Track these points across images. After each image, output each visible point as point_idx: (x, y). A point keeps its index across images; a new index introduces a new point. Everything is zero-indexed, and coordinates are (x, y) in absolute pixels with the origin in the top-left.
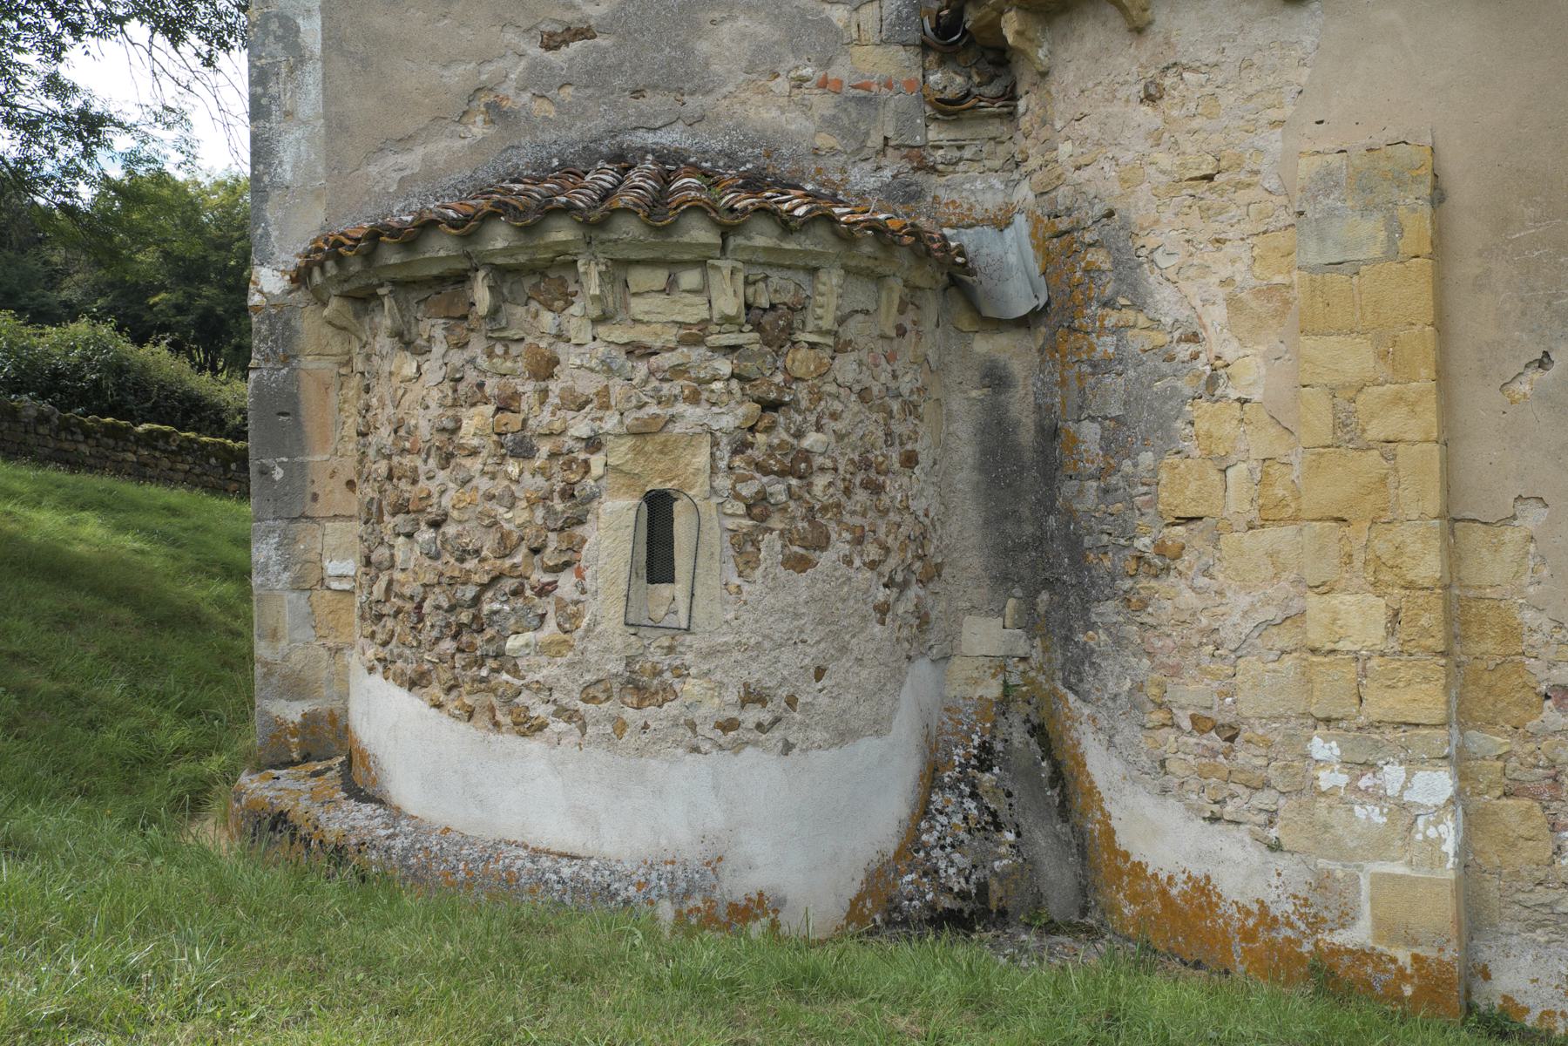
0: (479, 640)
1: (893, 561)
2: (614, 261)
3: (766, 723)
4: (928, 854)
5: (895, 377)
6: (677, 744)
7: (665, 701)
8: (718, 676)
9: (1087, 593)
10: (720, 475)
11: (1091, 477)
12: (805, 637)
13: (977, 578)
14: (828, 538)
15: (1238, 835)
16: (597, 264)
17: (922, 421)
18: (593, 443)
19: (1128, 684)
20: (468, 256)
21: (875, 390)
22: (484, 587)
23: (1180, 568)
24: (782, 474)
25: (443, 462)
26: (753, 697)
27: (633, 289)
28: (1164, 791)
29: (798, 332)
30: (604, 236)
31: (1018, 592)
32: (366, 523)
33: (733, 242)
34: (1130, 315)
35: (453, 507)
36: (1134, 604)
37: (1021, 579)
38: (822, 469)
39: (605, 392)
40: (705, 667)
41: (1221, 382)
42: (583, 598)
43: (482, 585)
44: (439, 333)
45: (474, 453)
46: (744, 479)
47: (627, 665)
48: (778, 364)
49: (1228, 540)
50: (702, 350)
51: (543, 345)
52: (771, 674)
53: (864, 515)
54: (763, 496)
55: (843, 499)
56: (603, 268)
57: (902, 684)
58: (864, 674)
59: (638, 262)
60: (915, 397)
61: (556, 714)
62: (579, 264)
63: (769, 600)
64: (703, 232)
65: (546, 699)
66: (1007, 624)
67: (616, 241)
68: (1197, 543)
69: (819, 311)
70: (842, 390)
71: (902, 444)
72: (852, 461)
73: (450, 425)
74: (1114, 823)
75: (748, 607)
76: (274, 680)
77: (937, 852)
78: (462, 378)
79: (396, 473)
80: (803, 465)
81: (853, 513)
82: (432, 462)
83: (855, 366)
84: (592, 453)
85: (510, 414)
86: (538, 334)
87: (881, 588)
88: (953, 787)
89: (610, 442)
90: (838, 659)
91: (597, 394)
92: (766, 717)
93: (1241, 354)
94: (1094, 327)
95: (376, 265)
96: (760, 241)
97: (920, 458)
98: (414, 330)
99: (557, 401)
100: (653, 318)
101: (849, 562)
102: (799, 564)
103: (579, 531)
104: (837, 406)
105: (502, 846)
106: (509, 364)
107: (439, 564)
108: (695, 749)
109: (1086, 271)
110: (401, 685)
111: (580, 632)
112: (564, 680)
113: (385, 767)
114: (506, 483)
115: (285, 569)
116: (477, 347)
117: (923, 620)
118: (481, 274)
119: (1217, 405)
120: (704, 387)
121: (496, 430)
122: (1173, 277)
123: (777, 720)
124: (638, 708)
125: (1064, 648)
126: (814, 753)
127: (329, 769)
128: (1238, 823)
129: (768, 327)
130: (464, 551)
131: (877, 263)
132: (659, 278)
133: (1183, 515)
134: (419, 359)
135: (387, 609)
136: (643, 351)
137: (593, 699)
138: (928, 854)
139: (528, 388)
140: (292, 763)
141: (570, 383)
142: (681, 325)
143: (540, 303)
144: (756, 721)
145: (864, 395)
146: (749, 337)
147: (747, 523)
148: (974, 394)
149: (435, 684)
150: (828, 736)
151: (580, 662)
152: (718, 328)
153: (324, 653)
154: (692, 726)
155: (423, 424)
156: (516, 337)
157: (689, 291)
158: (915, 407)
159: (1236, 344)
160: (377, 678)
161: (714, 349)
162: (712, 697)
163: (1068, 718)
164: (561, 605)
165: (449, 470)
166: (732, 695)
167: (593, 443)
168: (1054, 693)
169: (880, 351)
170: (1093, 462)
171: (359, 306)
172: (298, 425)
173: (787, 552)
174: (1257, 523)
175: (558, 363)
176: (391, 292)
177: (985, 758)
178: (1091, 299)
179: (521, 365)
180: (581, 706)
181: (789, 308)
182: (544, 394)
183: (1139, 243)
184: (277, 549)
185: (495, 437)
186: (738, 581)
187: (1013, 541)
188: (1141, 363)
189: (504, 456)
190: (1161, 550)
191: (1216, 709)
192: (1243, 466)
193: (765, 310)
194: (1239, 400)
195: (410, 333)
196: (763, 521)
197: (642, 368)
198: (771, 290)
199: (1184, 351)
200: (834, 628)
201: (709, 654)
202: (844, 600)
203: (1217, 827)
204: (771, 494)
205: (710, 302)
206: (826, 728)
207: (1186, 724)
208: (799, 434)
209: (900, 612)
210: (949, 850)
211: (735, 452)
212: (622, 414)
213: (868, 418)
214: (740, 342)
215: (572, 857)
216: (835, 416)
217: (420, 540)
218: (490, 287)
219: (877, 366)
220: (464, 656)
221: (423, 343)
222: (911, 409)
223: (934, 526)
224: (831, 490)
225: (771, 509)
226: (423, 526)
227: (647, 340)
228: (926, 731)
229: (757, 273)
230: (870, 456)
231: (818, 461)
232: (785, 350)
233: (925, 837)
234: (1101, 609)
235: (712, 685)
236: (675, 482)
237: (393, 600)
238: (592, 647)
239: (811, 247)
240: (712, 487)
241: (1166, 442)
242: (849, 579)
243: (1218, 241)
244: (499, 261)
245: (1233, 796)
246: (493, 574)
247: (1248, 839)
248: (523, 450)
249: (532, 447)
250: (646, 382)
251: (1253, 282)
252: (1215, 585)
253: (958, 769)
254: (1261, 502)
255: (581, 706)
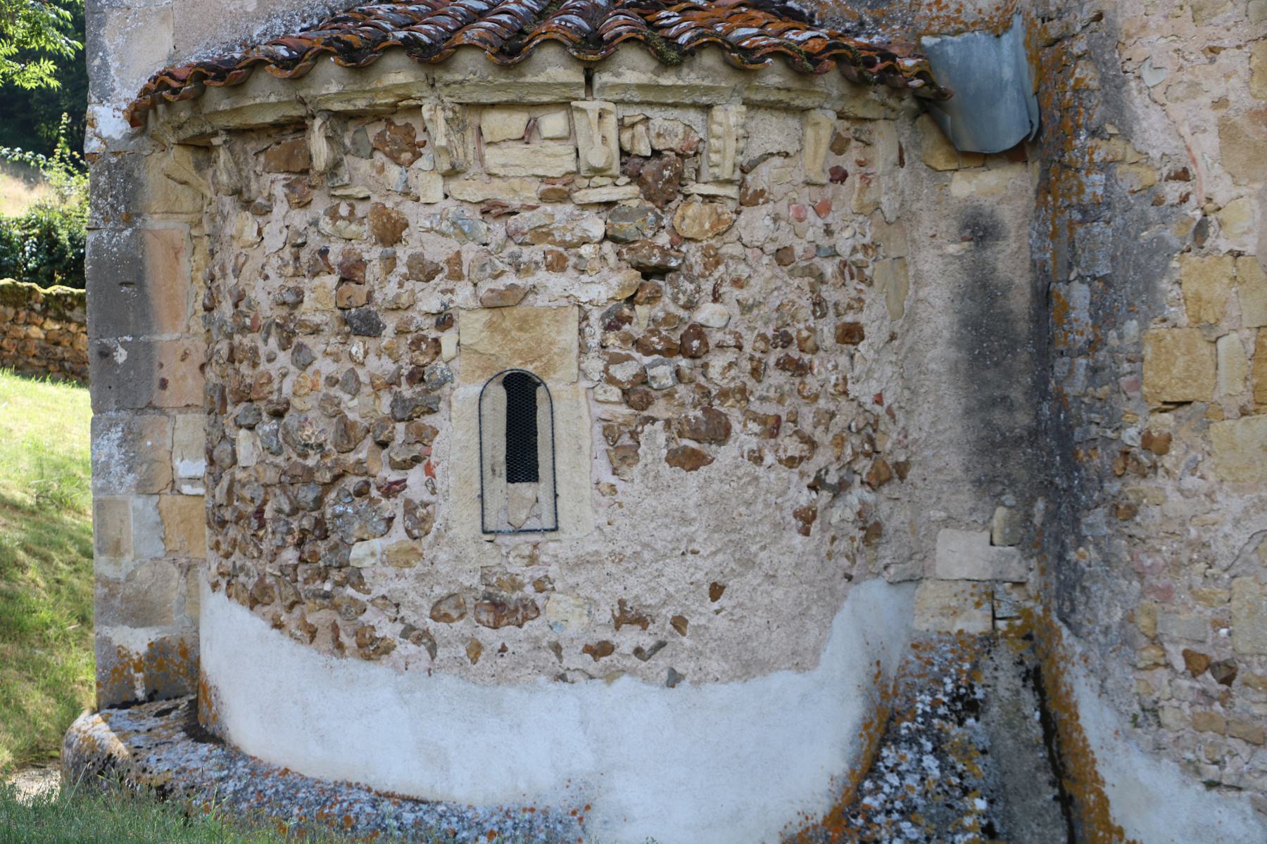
0: (322, 547)
1: (821, 458)
2: (466, 106)
3: (646, 648)
4: (869, 820)
5: (828, 232)
6: (540, 670)
7: (525, 618)
8: (587, 591)
9: (1077, 499)
10: (591, 354)
11: (1081, 353)
12: (695, 547)
13: (955, 481)
14: (728, 430)
15: (1239, 805)
16: (443, 109)
17: (871, 284)
18: (444, 321)
19: (1118, 615)
20: (302, 102)
21: (799, 250)
22: (327, 487)
23: (1167, 465)
24: (669, 352)
25: (284, 342)
26: (628, 617)
27: (487, 138)
28: (1158, 748)
29: (691, 183)
30: (448, 77)
31: (1009, 499)
32: (209, 414)
33: (602, 78)
34: (1117, 146)
35: (294, 394)
36: (1125, 512)
37: (1013, 483)
38: (720, 346)
39: (456, 260)
40: (571, 581)
41: (1211, 230)
42: (433, 498)
43: (325, 484)
44: (279, 191)
45: (316, 331)
46: (617, 359)
47: (482, 576)
48: (665, 222)
49: (1217, 428)
50: (569, 208)
51: (389, 205)
52: (652, 589)
53: (780, 401)
54: (642, 379)
55: (751, 383)
56: (450, 114)
57: (835, 610)
58: (778, 594)
59: (493, 106)
60: (860, 256)
61: (404, 634)
62: (424, 109)
63: (650, 502)
64: (562, 70)
65: (393, 616)
66: (996, 540)
67: (461, 83)
68: (1184, 433)
69: (715, 158)
70: (748, 251)
71: (838, 315)
72: (763, 337)
73: (290, 298)
74: (1107, 790)
75: (624, 510)
76: (116, 603)
77: (880, 818)
78: (304, 244)
79: (239, 355)
80: (696, 343)
81: (763, 399)
82: (273, 342)
83: (768, 222)
84: (443, 331)
85: (353, 285)
86: (384, 192)
87: (806, 491)
88: (912, 740)
89: (463, 319)
90: (741, 575)
91: (448, 262)
92: (647, 641)
93: (1234, 194)
94: (1083, 163)
95: (206, 110)
96: (630, 77)
97: (866, 331)
98: (254, 186)
99: (404, 270)
100: (511, 172)
101: (757, 459)
102: (690, 460)
103: (427, 420)
104: (743, 271)
105: (344, 790)
106: (354, 227)
107: (280, 460)
108: (562, 678)
109: (1076, 91)
110: (242, 604)
111: (430, 537)
112: (412, 595)
113: (224, 700)
114: (351, 365)
115: (130, 470)
116: (320, 204)
117: (872, 532)
118: (318, 122)
119: (1207, 259)
120: (573, 251)
121: (340, 305)
122: (1162, 99)
123: (661, 645)
124: (495, 628)
125: (1058, 569)
126: (709, 687)
127: (176, 708)
128: (1240, 789)
129: (650, 179)
130: (306, 445)
131: (793, 95)
132: (516, 122)
133: (1169, 399)
134: (260, 220)
135: (228, 514)
136: (499, 210)
137: (447, 618)
138: (869, 820)
139: (373, 254)
140: (137, 702)
141: (419, 250)
142: (543, 179)
143: (385, 154)
144: (634, 645)
145: (782, 256)
146: (626, 192)
147: (624, 410)
148: (952, 249)
149: (277, 601)
150: (727, 667)
151: (429, 573)
152: (586, 181)
153: (175, 572)
154: (557, 648)
155: (263, 297)
156: (361, 195)
157: (552, 139)
158: (860, 268)
159: (1228, 180)
160: (221, 596)
161: (584, 206)
162: (581, 616)
163: (1062, 658)
164: (410, 508)
165: (290, 351)
166: (605, 614)
167: (444, 321)
168: (1049, 627)
169: (805, 201)
170: (1082, 334)
171: (201, 156)
172: (143, 299)
173: (673, 446)
174: (1251, 407)
175: (407, 225)
176: (225, 142)
177: (967, 705)
178: (1078, 126)
179: (366, 229)
180: (431, 625)
181: (677, 154)
182: (390, 263)
183: (1126, 55)
184: (120, 446)
185: (339, 312)
186: (613, 480)
187: (1003, 435)
188: (1128, 208)
189: (348, 334)
190: (1147, 441)
191: (1209, 641)
192: (1234, 336)
193: (646, 158)
194: (1230, 252)
195: (249, 190)
196: (643, 409)
197: (498, 229)
198: (653, 133)
199: (1172, 191)
200: (735, 537)
201: (577, 565)
202: (748, 504)
203: (1214, 792)
204: (653, 378)
205: (577, 150)
206: (725, 657)
207: (1180, 664)
208: (690, 306)
209: (834, 520)
210: (896, 816)
211: (608, 328)
212: (475, 285)
213: (788, 285)
214: (613, 198)
215: (417, 802)
216: (738, 283)
217: (260, 432)
218: (328, 138)
219: (801, 220)
220: (306, 567)
221: (264, 202)
222: (851, 270)
223: (893, 416)
224: (733, 372)
225: (653, 393)
226: (265, 417)
227: (504, 197)
228: (875, 670)
229: (633, 113)
230: (790, 330)
231: (715, 338)
232: (673, 205)
233: (867, 800)
234: (1090, 520)
235: (581, 601)
236: (536, 364)
237: (236, 503)
238: (443, 556)
239: (698, 82)
240: (580, 369)
241: (1150, 309)
242: (756, 479)
243: (1212, 50)
244: (337, 107)
245: (1233, 755)
246: (337, 471)
247: (1249, 810)
248: (368, 326)
249: (379, 323)
250: (503, 247)
251: (1249, 102)
252: (1203, 486)
253: (920, 720)
254: (1255, 381)
255: (431, 625)
